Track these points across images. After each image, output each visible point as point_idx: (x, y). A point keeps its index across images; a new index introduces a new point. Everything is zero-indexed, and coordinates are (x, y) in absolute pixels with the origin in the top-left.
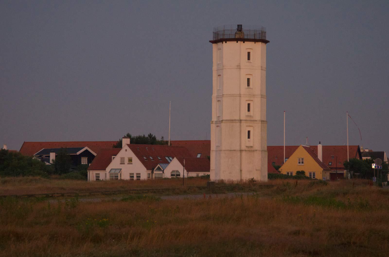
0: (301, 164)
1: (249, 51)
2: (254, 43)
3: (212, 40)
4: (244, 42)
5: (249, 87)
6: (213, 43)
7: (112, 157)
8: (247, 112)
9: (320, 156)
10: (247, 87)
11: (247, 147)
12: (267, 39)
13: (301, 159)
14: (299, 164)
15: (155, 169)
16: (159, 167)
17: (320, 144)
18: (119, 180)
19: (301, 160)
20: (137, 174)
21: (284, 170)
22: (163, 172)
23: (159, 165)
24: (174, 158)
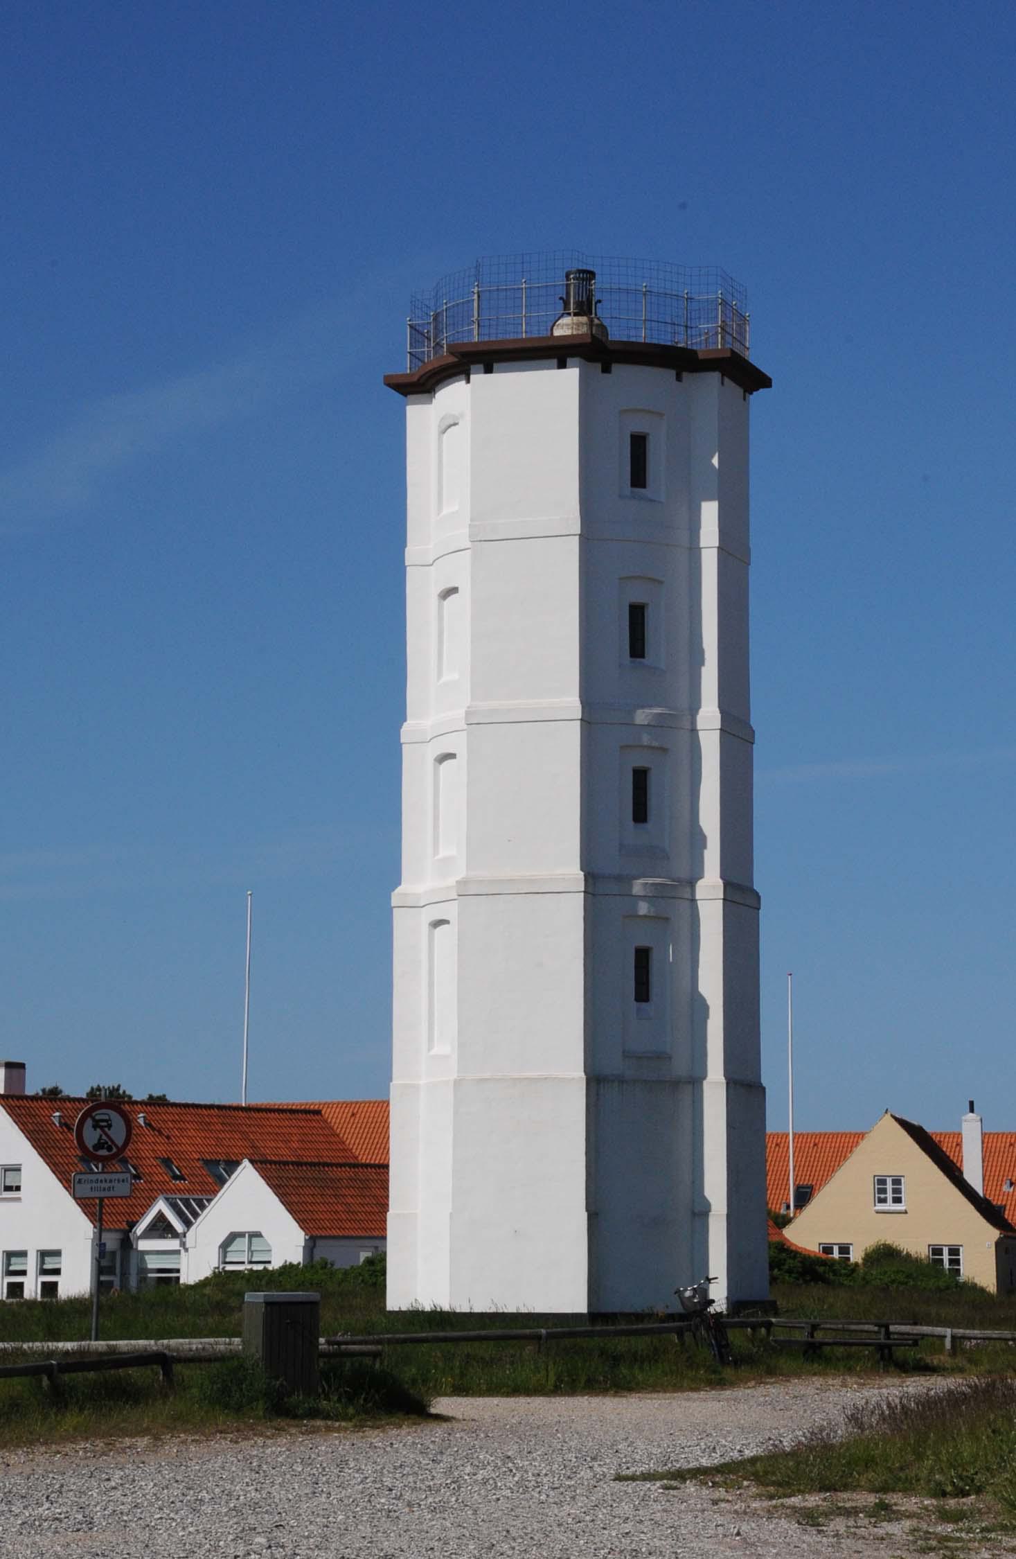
0: (890, 1206)
1: (640, 427)
2: (672, 373)
3: (405, 368)
4: (606, 370)
5: (642, 490)
6: (405, 394)
7: (151, 1201)
8: (632, 823)
9: (973, 1174)
10: (628, 489)
11: (626, 1055)
12: (757, 357)
13: (889, 1181)
14: (881, 1207)
15: (141, 1228)
16: (161, 1217)
17: (972, 1110)
18: (957, 1282)
19: (889, 1187)
20: (44, 1254)
21: (807, 1233)
22: (183, 1244)
23: (161, 1206)
24: (238, 1163)
